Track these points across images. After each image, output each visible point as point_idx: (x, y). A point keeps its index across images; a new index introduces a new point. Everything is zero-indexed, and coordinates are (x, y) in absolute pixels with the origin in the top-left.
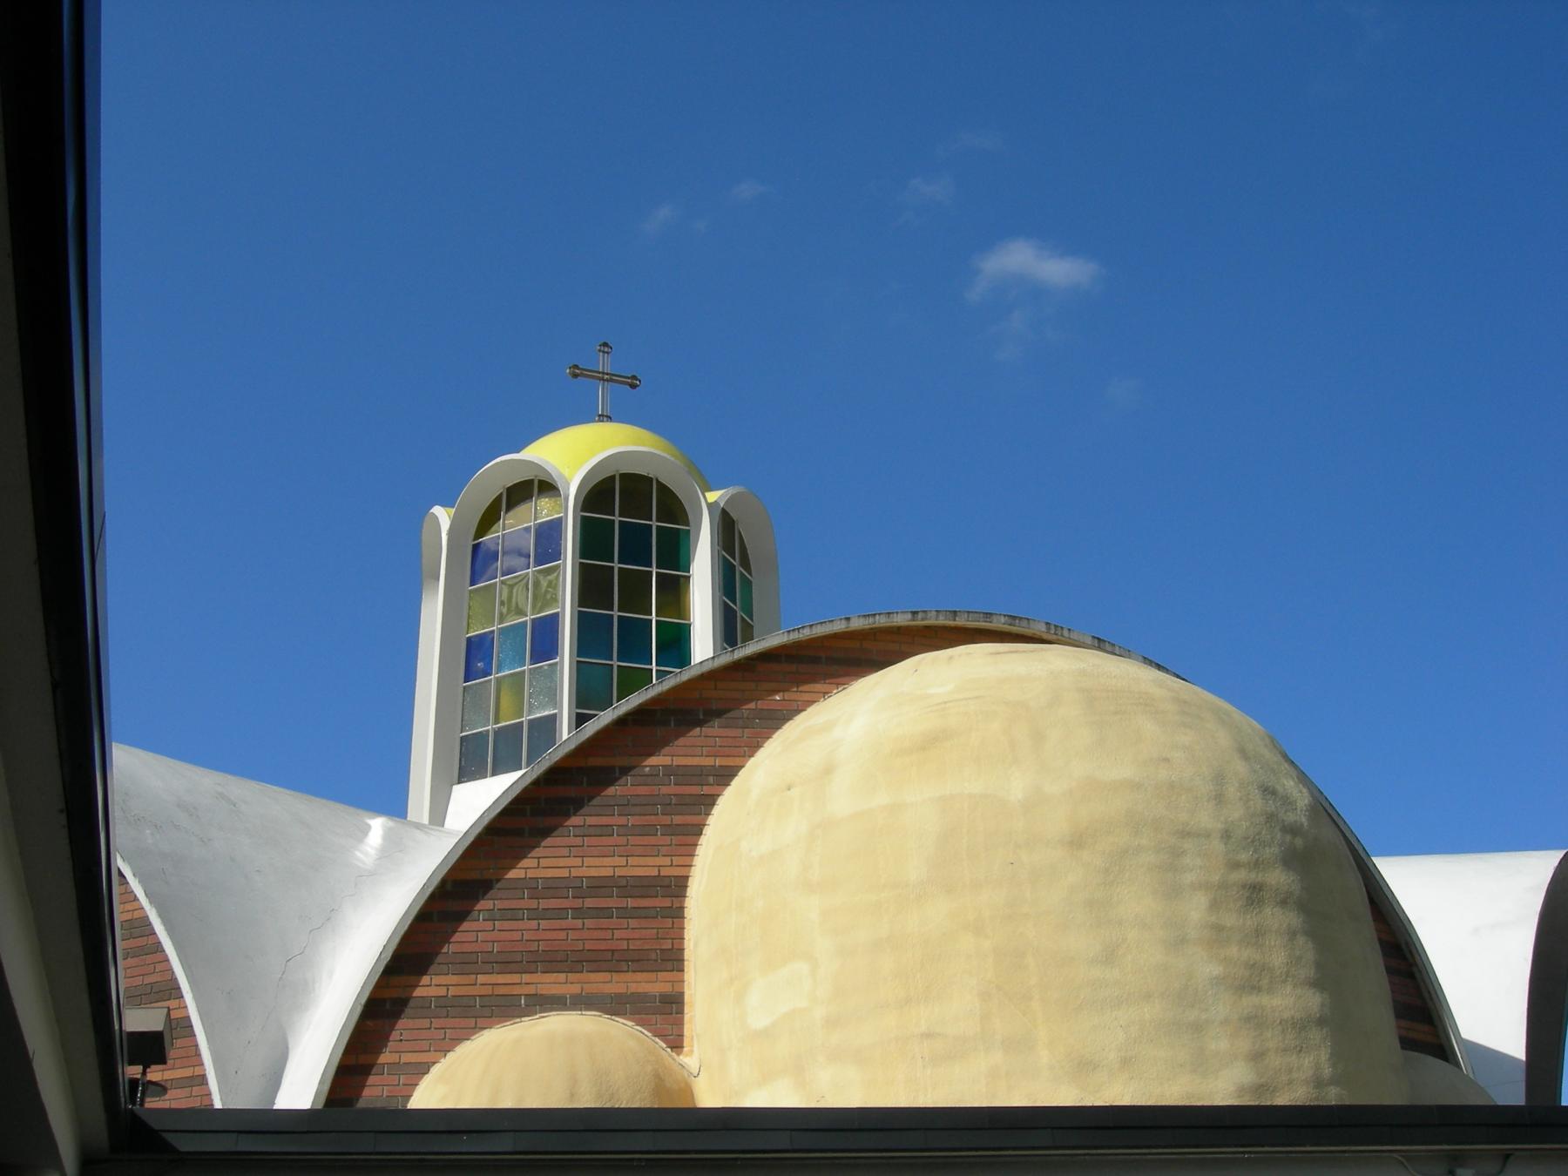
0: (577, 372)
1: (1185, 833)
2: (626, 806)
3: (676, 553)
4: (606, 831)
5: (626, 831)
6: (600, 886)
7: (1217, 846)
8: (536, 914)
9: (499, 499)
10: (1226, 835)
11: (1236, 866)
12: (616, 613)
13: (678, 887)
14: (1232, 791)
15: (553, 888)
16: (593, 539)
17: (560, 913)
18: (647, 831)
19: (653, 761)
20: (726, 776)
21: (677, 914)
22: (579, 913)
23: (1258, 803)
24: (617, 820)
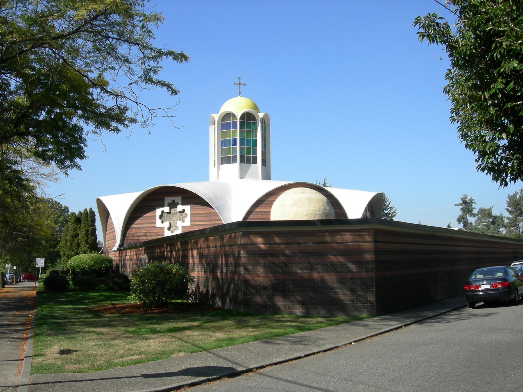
0: (235, 84)
1: (316, 214)
2: (265, 204)
3: (255, 124)
4: (263, 206)
5: (265, 206)
6: (262, 212)
7: (319, 215)
8: (256, 214)
9: (225, 115)
10: (319, 214)
11: (320, 217)
12: (252, 156)
13: (270, 212)
14: (321, 210)
15: (258, 212)
16: (242, 125)
17: (259, 214)
18: (267, 206)
19: (268, 199)
20: (274, 201)
21: (270, 215)
22: (260, 214)
23: (323, 211)
24: (264, 205)
